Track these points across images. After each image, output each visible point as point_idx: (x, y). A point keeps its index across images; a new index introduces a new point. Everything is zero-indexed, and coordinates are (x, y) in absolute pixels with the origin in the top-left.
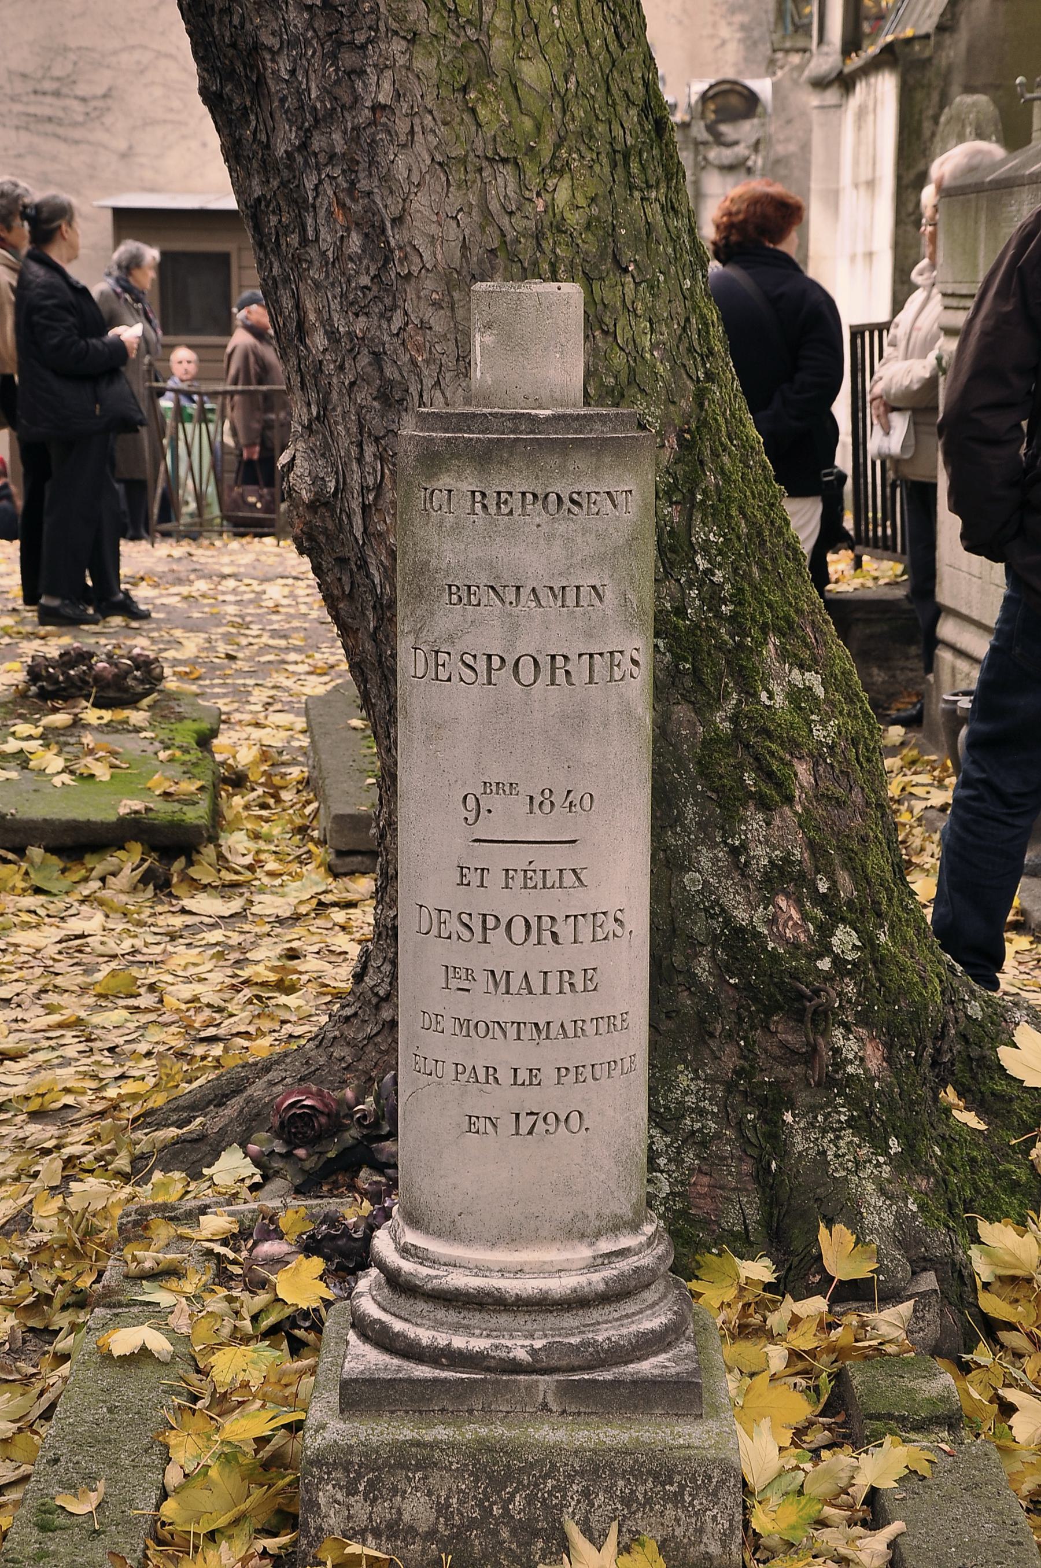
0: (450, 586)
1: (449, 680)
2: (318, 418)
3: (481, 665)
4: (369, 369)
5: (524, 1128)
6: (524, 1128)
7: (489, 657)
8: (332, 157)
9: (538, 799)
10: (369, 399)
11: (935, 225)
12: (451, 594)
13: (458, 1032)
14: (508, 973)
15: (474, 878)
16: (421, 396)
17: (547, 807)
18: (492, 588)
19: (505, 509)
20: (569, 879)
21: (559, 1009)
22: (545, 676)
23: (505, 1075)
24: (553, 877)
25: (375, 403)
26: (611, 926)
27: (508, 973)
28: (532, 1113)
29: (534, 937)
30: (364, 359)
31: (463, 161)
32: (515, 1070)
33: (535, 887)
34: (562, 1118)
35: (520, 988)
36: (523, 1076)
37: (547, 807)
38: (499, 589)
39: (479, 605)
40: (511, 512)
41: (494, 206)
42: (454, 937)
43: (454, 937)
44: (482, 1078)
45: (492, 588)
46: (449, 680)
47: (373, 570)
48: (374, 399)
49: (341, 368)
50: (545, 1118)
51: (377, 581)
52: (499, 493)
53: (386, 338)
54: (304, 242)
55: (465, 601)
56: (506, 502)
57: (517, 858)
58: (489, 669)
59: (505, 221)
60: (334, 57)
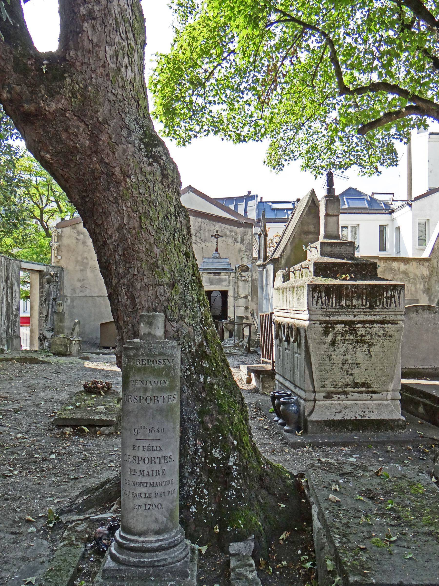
3: (138, 399)
5: (147, 508)
6: (147, 508)
8: (124, 284)
11: (434, 475)
15: (136, 448)
21: (157, 480)
22: (153, 401)
23: (143, 496)
24: (155, 448)
26: (169, 459)
31: (152, 285)
36: (147, 495)
41: (158, 294)
54: (119, 302)
57: (146, 444)
59: (160, 297)
60: (125, 265)
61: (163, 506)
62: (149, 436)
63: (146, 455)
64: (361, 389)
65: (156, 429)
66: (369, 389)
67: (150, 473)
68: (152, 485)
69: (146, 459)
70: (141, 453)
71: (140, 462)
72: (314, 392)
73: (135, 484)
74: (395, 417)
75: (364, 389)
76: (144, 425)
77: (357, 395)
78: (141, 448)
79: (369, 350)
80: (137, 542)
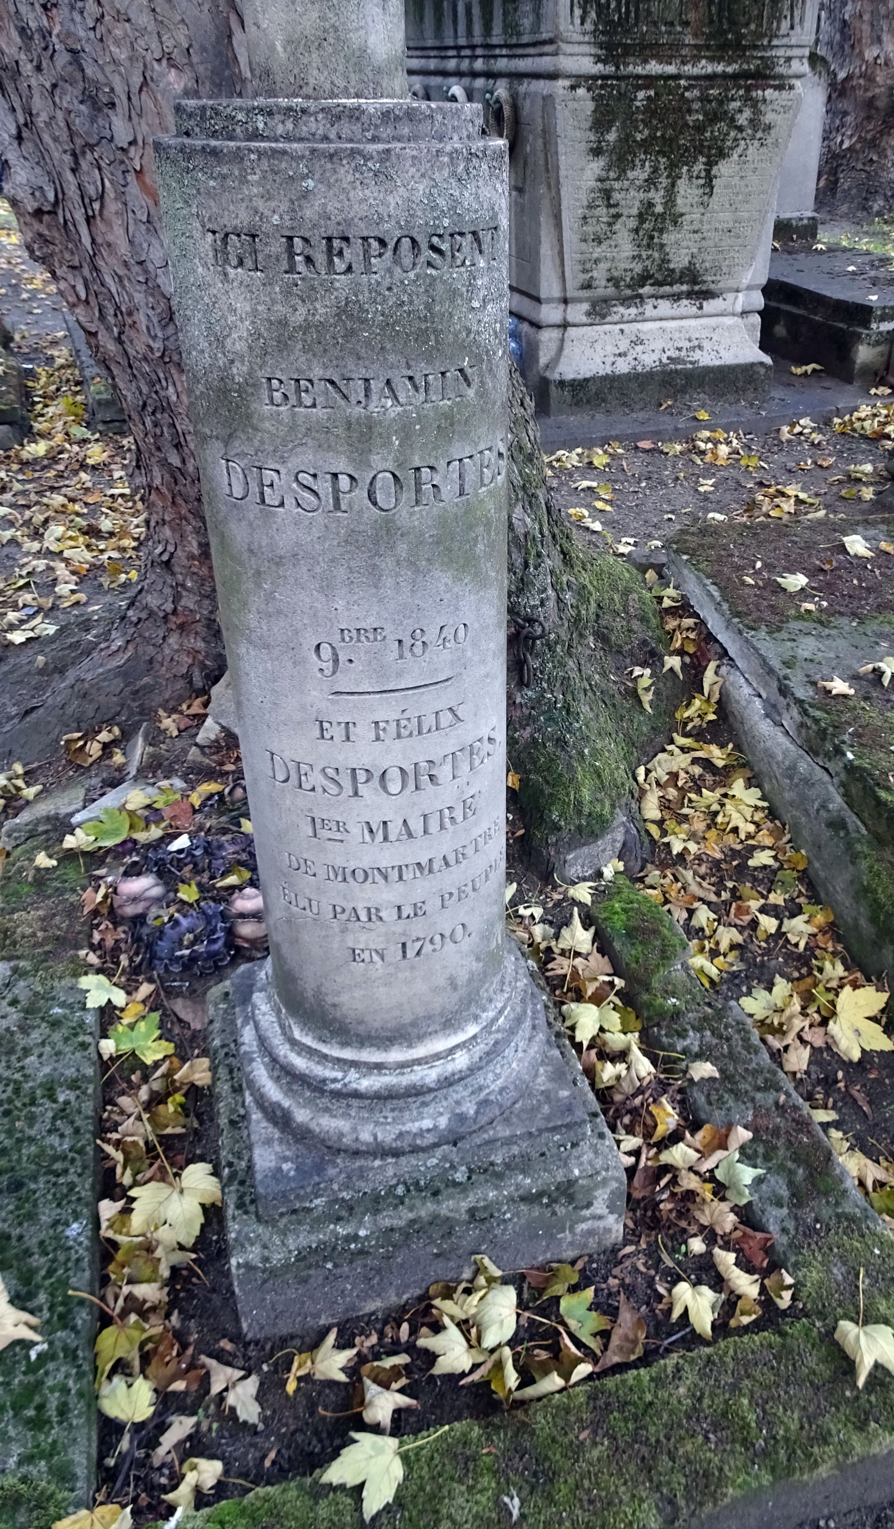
0: (269, 379)
1: (282, 504)
2: (26, 125)
3: (324, 486)
4: (70, 69)
7: (335, 475)
9: (408, 641)
10: (76, 102)
12: (271, 390)
13: (332, 876)
14: (385, 823)
15: (338, 732)
16: (129, 99)
17: (418, 649)
18: (332, 382)
19: (340, 265)
20: (446, 718)
22: (408, 495)
24: (429, 721)
25: (83, 107)
27: (385, 823)
28: (418, 939)
29: (411, 786)
30: (62, 58)
32: (399, 908)
33: (411, 735)
34: (447, 934)
35: (400, 834)
36: (407, 910)
37: (418, 649)
38: (342, 384)
39: (314, 406)
40: (349, 269)
42: (319, 790)
43: (319, 790)
44: (364, 917)
45: (332, 382)
46: (282, 504)
47: (108, 280)
48: (81, 102)
49: (39, 68)
50: (432, 941)
51: (114, 290)
52: (329, 239)
53: (82, 34)
55: (293, 400)
56: (340, 254)
58: (336, 491)
61: (470, 929)
62: (399, 675)
63: (393, 755)
64: (677, 288)
65: (431, 635)
66: (697, 288)
67: (416, 825)
68: (424, 868)
69: (394, 774)
70: (365, 753)
71: (362, 789)
72: (565, 301)
73: (345, 875)
74: (750, 360)
75: (685, 288)
76: (370, 622)
77: (665, 307)
78: (363, 732)
79: (708, 172)
80: (379, 1067)
